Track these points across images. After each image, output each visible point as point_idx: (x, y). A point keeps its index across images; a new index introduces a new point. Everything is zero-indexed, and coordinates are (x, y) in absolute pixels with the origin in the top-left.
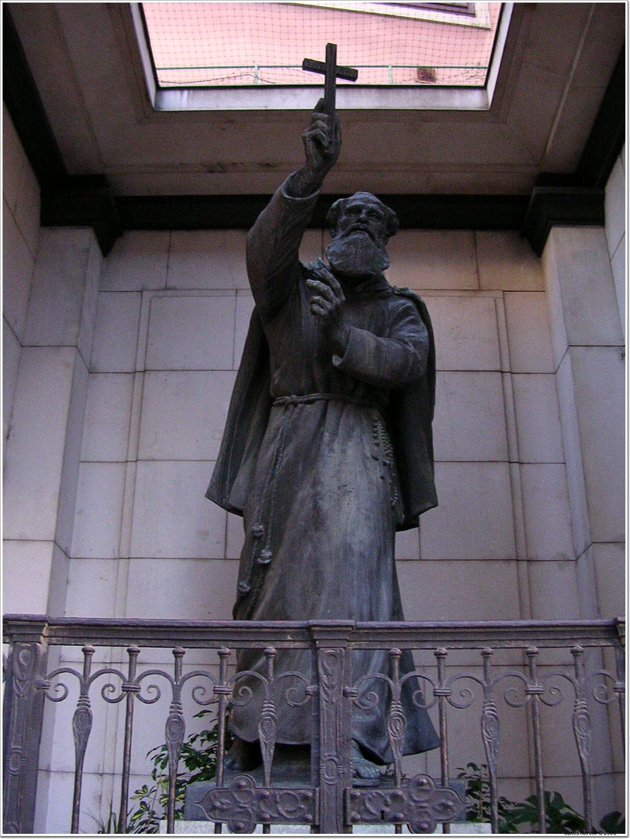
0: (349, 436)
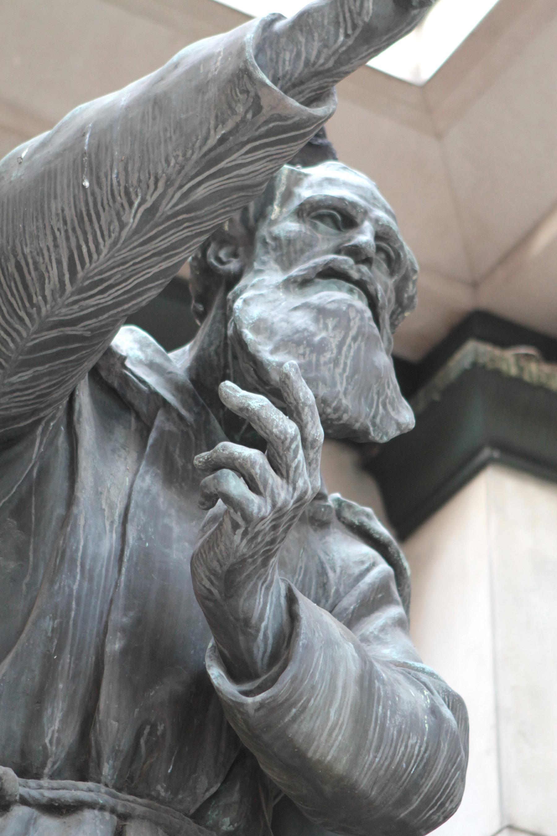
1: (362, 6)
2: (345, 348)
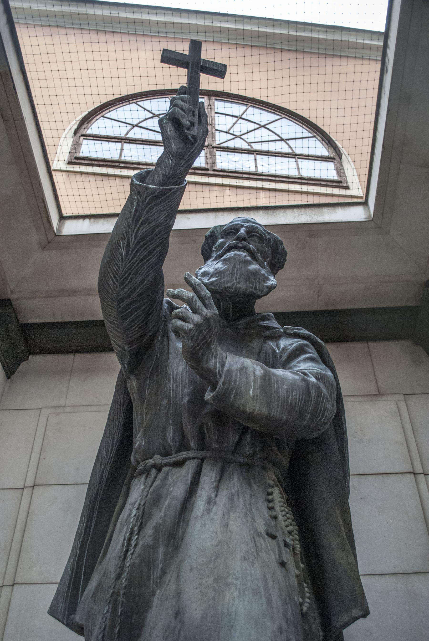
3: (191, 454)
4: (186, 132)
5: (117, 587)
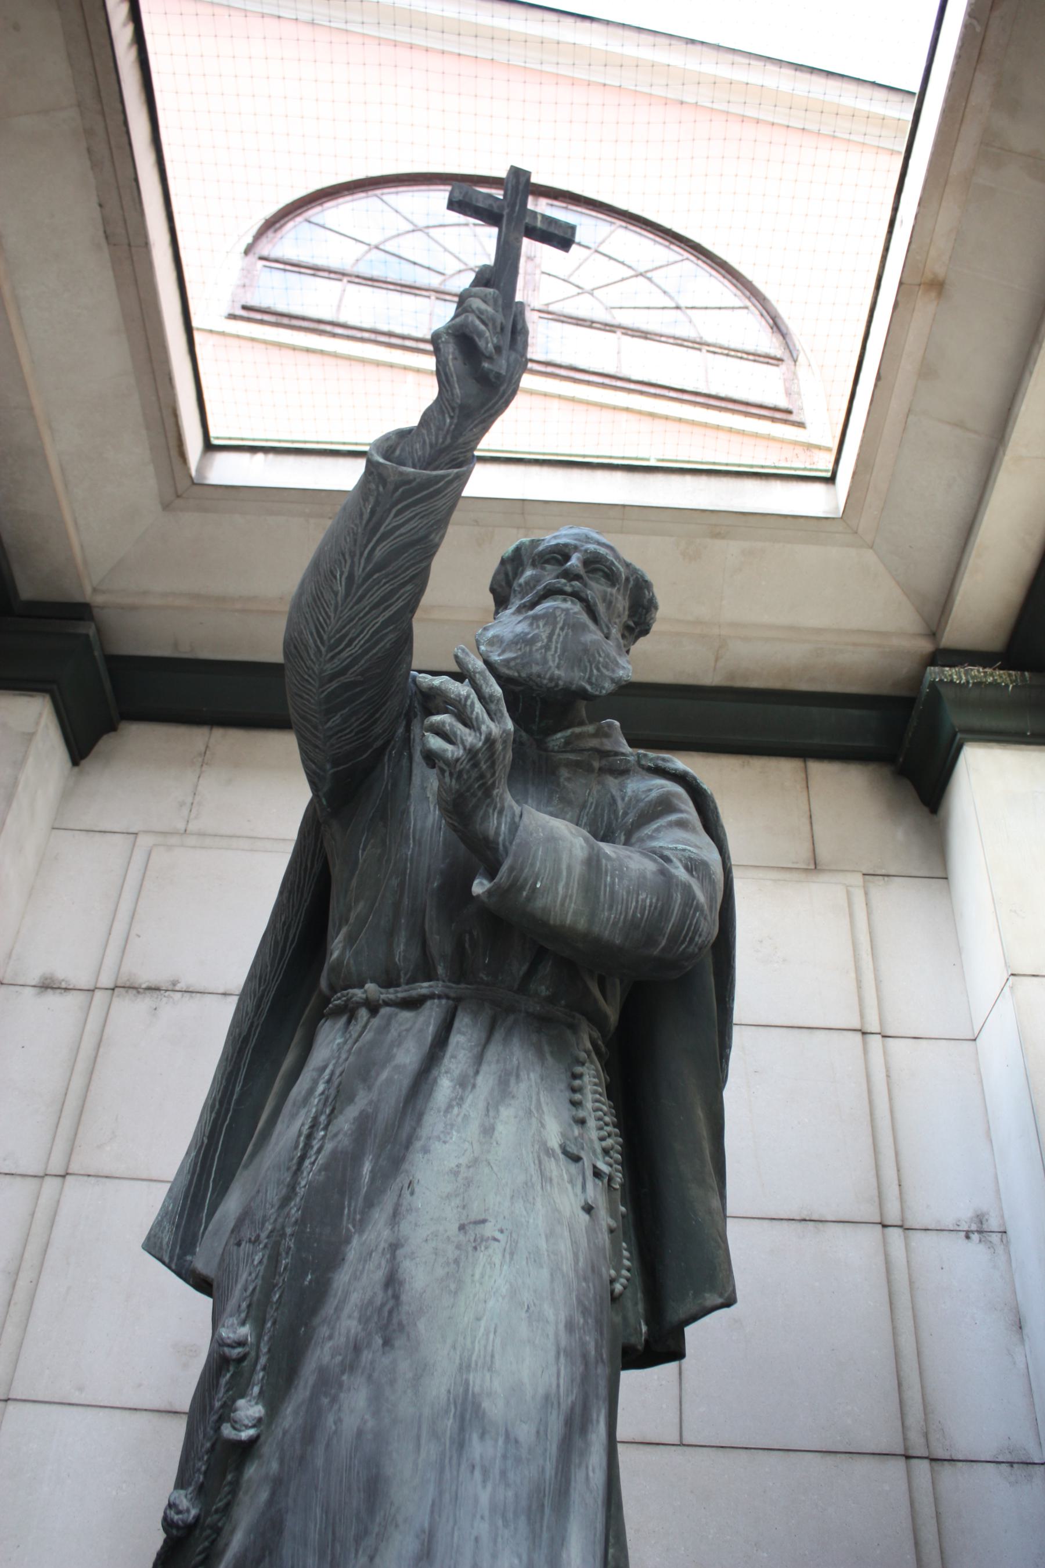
0: (503, 1090)
1: (453, 394)
2: (555, 637)
3: (437, 987)
4: (481, 358)
5: (280, 1220)
